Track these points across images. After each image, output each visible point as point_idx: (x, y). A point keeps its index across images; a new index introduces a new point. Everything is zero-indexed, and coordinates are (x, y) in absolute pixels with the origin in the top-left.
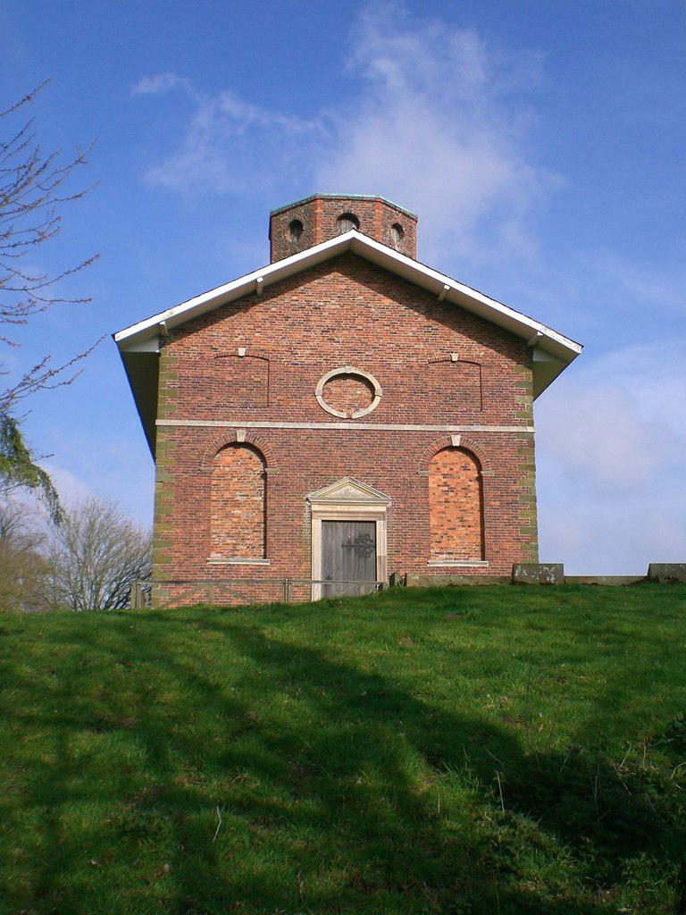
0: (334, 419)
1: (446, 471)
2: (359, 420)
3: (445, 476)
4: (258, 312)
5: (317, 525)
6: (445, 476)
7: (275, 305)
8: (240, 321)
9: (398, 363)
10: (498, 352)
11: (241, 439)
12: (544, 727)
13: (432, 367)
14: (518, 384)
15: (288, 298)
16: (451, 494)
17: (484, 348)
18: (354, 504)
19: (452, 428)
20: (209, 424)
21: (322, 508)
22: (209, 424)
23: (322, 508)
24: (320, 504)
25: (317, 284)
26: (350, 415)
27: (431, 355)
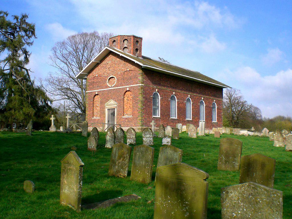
0: (110, 87)
1: (127, 96)
2: (113, 87)
3: (127, 97)
4: (99, 67)
5: (106, 110)
6: (127, 97)
7: (101, 65)
8: (97, 69)
9: (119, 73)
10: (136, 67)
11: (128, 90)
12: (87, 177)
13: (125, 73)
14: (139, 74)
15: (104, 62)
16: (128, 101)
17: (134, 66)
18: (112, 105)
19: (127, 86)
20: (92, 91)
21: (108, 106)
22: (92, 91)
23: (108, 106)
24: (107, 106)
25: (108, 59)
26: (111, 86)
27: (124, 70)
